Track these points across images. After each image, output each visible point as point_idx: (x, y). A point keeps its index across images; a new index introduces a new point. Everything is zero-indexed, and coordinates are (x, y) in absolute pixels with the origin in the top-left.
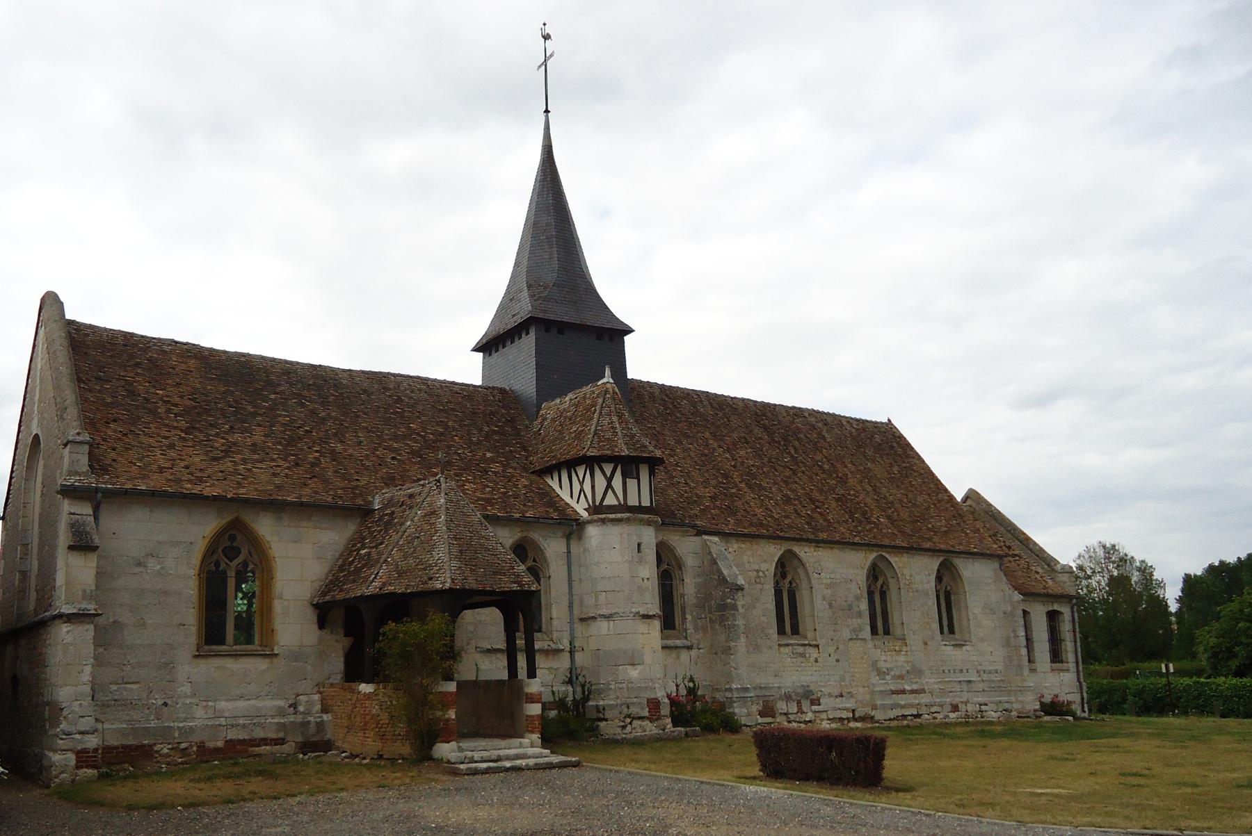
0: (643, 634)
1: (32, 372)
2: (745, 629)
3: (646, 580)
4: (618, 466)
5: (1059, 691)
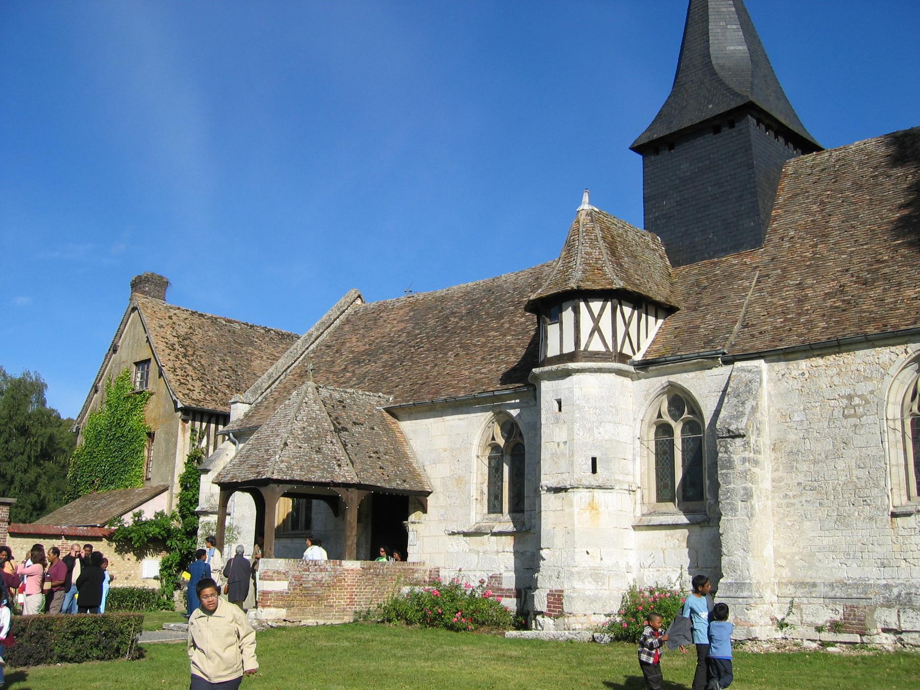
0: (555, 511)
1: (688, 37)
2: (744, 494)
3: (562, 445)
4: (579, 307)
5: (886, 513)
